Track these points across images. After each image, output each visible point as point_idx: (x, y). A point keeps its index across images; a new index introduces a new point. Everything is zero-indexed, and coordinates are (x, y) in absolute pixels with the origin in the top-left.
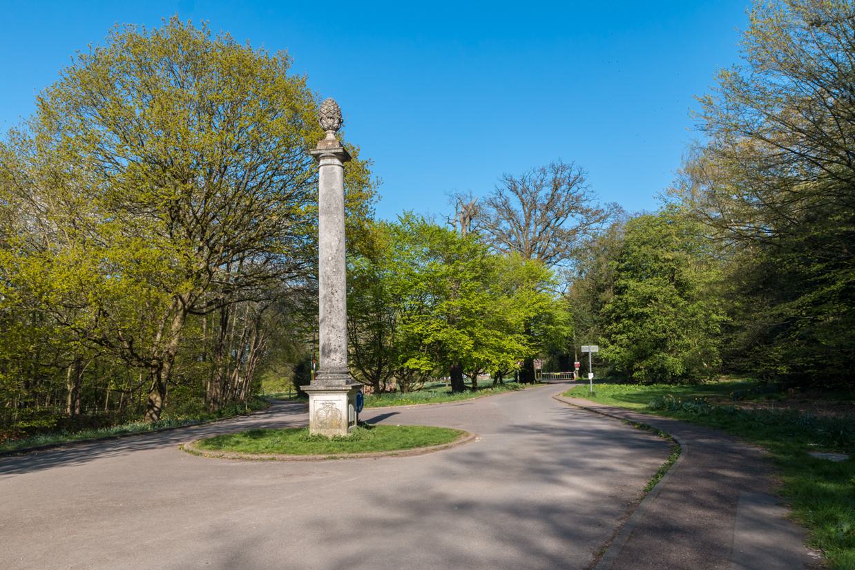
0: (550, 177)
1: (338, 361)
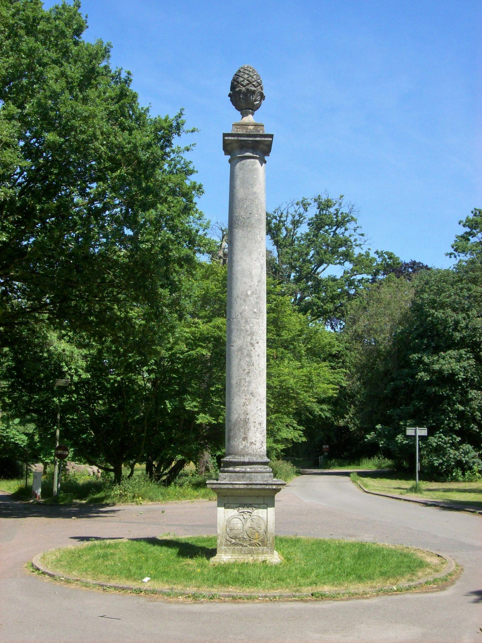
0: (313, 212)
1: (258, 445)
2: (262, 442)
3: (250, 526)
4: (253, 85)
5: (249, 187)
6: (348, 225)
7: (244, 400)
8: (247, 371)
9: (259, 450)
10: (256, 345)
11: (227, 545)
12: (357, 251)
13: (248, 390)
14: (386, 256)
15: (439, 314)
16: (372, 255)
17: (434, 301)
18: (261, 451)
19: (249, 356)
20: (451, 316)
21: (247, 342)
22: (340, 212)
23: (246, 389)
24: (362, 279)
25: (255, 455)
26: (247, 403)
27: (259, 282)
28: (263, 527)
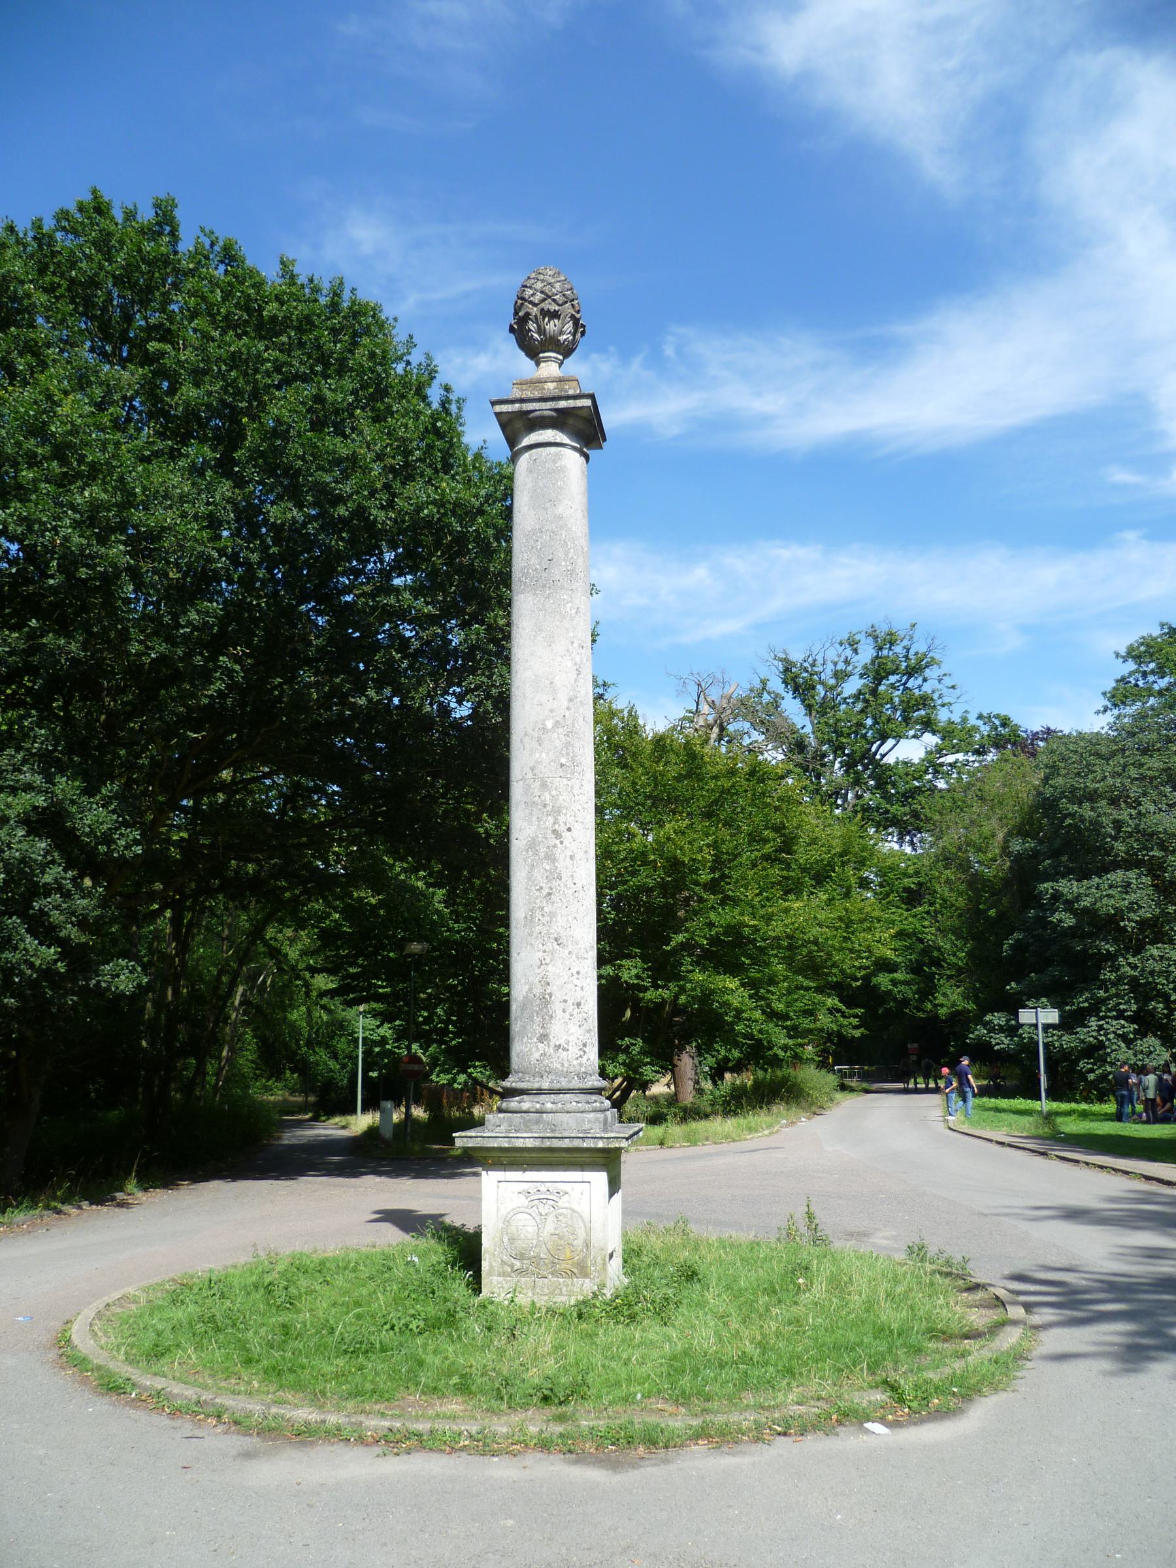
0: (867, 653)
1: (574, 1051)
2: (585, 1045)
3: (553, 1231)
4: (554, 300)
5: (548, 505)
6: (927, 672)
7: (541, 954)
8: (545, 891)
9: (575, 1062)
10: (566, 834)
11: (503, 1274)
12: (943, 716)
13: (548, 933)
14: (997, 722)
15: (1086, 811)
16: (973, 721)
17: (1074, 789)
18: (581, 1065)
19: (551, 858)
20: (1107, 814)
21: (546, 828)
22: (912, 652)
23: (544, 930)
24: (957, 761)
25: (566, 1074)
26: (548, 961)
27: (571, 700)
28: (582, 1235)
